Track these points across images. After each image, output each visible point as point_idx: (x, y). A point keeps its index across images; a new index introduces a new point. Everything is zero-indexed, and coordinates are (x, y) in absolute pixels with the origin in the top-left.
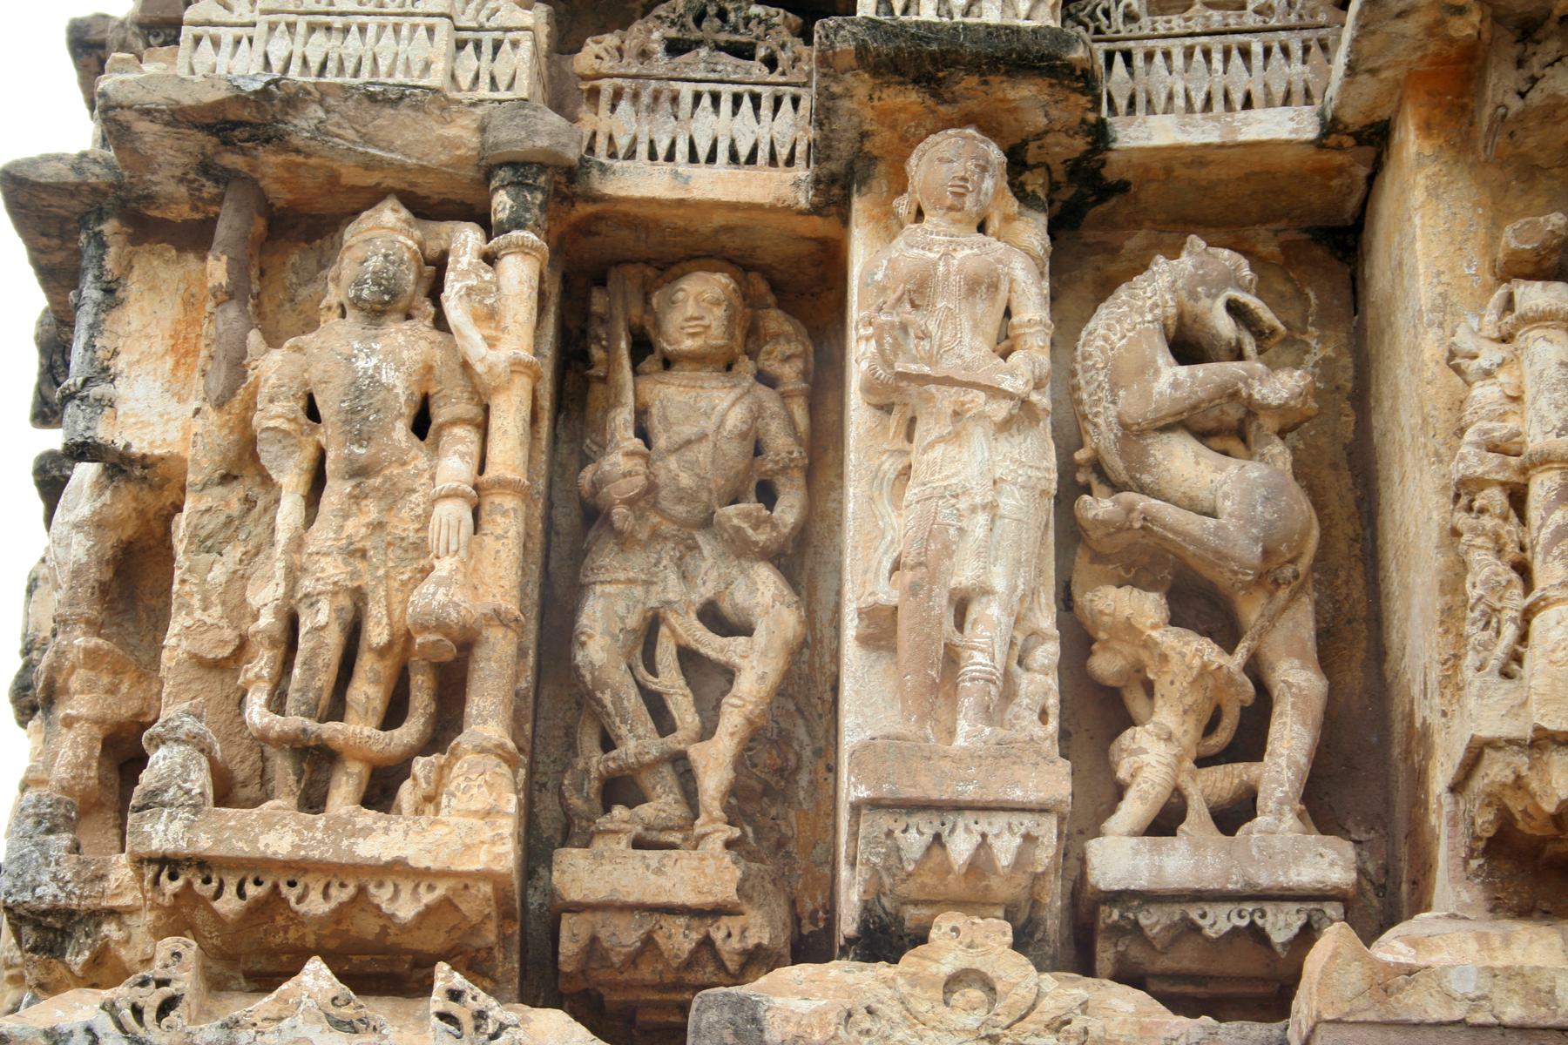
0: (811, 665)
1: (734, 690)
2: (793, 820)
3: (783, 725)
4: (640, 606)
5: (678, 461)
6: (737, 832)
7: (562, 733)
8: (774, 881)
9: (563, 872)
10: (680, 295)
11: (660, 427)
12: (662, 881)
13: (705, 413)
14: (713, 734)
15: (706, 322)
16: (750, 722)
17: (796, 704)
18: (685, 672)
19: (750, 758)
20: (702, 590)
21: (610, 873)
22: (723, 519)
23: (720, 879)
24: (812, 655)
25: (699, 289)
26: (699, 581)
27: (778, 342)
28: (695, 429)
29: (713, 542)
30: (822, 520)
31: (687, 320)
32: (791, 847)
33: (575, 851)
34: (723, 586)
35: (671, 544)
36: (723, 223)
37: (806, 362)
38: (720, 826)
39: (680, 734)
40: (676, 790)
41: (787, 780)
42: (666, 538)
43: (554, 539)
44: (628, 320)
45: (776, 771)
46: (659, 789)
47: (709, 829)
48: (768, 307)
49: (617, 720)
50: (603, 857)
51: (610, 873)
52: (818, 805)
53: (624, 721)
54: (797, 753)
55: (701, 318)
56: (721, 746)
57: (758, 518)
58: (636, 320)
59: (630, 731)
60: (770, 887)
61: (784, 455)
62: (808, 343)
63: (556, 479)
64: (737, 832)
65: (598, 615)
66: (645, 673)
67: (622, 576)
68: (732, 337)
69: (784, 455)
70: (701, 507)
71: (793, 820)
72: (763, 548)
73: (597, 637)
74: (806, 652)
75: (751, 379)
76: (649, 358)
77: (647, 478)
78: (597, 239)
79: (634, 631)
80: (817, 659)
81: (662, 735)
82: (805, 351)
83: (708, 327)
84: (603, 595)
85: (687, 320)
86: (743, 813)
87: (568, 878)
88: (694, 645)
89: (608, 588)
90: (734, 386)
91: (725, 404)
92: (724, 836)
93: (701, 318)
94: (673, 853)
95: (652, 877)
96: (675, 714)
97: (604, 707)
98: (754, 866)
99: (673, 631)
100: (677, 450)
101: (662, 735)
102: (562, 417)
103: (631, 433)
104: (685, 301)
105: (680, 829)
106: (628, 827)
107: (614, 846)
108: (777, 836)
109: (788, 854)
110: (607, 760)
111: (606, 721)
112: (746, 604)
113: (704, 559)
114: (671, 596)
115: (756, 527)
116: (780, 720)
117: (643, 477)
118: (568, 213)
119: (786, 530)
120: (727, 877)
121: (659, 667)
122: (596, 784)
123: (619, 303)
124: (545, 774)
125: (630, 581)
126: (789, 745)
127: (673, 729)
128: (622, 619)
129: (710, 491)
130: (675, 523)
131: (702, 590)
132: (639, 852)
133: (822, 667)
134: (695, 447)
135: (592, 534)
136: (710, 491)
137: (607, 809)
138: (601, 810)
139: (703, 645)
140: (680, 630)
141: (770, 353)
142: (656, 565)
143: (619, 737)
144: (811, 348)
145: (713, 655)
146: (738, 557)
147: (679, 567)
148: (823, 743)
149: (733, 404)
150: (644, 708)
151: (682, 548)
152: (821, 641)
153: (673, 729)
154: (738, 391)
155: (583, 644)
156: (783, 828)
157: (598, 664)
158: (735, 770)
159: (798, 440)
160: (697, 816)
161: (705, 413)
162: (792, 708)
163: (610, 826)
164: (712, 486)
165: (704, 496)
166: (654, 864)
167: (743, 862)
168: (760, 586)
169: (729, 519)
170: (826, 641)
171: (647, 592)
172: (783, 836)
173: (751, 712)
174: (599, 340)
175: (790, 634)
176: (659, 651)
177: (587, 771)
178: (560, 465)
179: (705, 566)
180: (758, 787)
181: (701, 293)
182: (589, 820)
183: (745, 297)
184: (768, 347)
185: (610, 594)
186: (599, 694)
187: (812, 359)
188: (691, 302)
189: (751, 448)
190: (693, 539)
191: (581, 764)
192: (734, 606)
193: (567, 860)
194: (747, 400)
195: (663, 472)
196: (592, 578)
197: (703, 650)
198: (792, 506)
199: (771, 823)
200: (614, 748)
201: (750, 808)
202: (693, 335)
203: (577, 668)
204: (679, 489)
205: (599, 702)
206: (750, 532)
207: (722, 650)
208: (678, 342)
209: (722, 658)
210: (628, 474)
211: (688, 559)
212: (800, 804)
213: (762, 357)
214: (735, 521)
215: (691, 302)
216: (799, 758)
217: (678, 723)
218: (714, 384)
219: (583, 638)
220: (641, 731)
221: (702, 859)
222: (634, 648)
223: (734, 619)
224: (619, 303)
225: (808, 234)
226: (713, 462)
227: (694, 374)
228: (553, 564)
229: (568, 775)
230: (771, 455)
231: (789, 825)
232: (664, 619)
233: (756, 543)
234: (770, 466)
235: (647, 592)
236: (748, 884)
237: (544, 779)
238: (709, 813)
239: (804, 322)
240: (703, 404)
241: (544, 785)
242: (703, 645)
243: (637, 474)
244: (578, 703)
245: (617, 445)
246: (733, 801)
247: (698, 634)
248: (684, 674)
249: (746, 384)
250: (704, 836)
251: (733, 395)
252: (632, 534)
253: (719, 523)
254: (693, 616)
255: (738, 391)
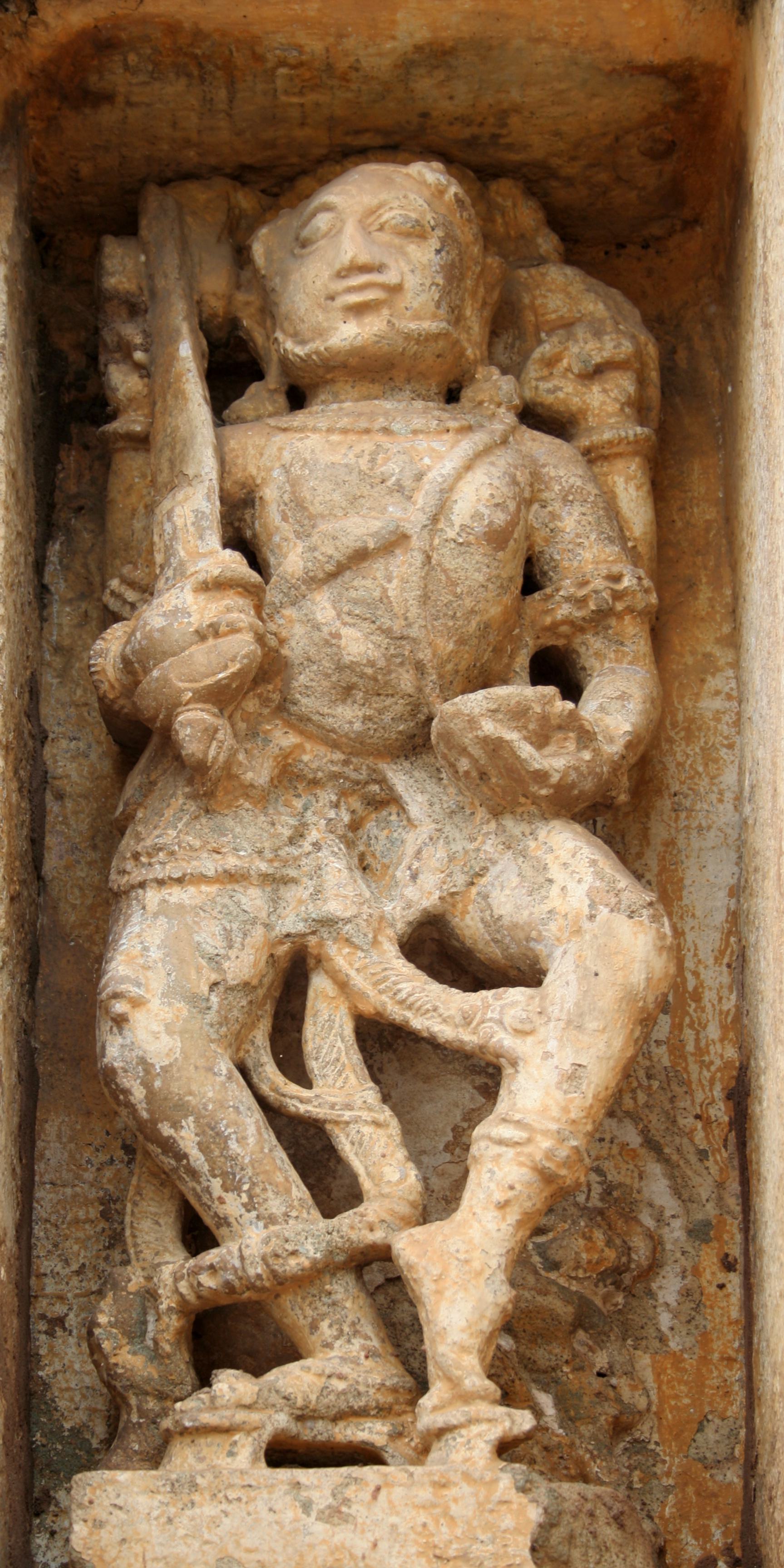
0: (676, 1048)
1: (502, 1105)
2: (649, 1376)
3: (613, 1176)
4: (259, 932)
5: (335, 603)
6: (524, 1421)
7: (94, 1212)
8: (618, 1520)
9: (99, 1524)
10: (322, 221)
11: (287, 529)
12: (343, 1535)
13: (399, 488)
14: (533, 1549)
15: (390, 277)
16: (546, 1177)
17: (645, 1132)
18: (375, 1072)
19: (541, 1250)
20: (411, 892)
21: (214, 1522)
22: (456, 726)
23: (488, 1526)
24: (678, 1027)
25: (368, 200)
26: (402, 874)
27: (571, 336)
28: (376, 525)
29: (431, 786)
30: (689, 738)
31: (341, 275)
32: (645, 1430)
33: (123, 1476)
34: (461, 879)
35: (328, 795)
36: (422, 35)
37: (641, 382)
38: (484, 1409)
39: (370, 1209)
40: (368, 1329)
41: (630, 1293)
42: (314, 783)
43: (53, 806)
44: (198, 304)
45: (603, 1276)
46: (326, 1329)
47: (454, 1415)
48: (542, 261)
49: (216, 1184)
50: (194, 1486)
51: (214, 1522)
52: (705, 1339)
53: (232, 1185)
54: (650, 1236)
55: (379, 268)
56: (475, 1232)
57: (544, 718)
58: (216, 305)
59: (249, 1207)
60: (609, 1533)
61: (598, 583)
62: (644, 337)
63: (49, 679)
64: (524, 1421)
65: (155, 954)
66: (279, 1079)
67: (209, 865)
68: (457, 318)
69: (598, 583)
70: (399, 707)
71: (649, 1376)
72: (559, 788)
73: (155, 1004)
74: (665, 1022)
75: (510, 419)
76: (254, 388)
77: (260, 639)
78: (107, 116)
79: (246, 986)
80: (689, 1035)
81: (328, 1213)
82: (639, 354)
83: (396, 289)
84: (164, 909)
85: (341, 275)
86: (529, 1365)
87: (108, 1537)
88: (396, 1013)
89: (176, 895)
90: (468, 429)
91: (449, 466)
92: (495, 1433)
93: (379, 268)
94: (370, 1473)
95: (320, 1529)
96: (357, 1165)
97: (181, 1156)
98: (570, 1490)
99: (343, 985)
100: (332, 576)
101: (328, 1213)
102: (55, 548)
103: (214, 540)
104: (334, 232)
105: (382, 1411)
106: (255, 1417)
107: (223, 1462)
108: (611, 1410)
109: (640, 1448)
110: (195, 1272)
111: (188, 1186)
112: (524, 916)
113: (411, 823)
114: (334, 907)
115: (541, 740)
116: (607, 1165)
117: (247, 637)
118: (22, 35)
119: (614, 749)
120: (508, 1522)
121: (313, 1065)
122: (174, 1322)
123: (171, 260)
124: (61, 1298)
125: (231, 877)
126: (631, 1218)
127: (355, 1197)
128: (214, 960)
129: (420, 668)
130: (335, 746)
131: (411, 892)
132: (284, 1474)
133: (700, 1051)
134: (378, 567)
135: (135, 779)
136: (420, 668)
137: (204, 1381)
138: (189, 1377)
139: (419, 1011)
140: (358, 981)
141: (550, 363)
142: (291, 841)
143: (224, 1221)
144: (652, 350)
145: (445, 1032)
146: (496, 813)
147: (350, 844)
148: (711, 1210)
149: (468, 467)
150: (281, 1155)
151: (355, 803)
152: (697, 997)
153: (355, 1197)
154: (479, 439)
155: (120, 1021)
156: (626, 1394)
157: (159, 1063)
158: (512, 1283)
159: (633, 556)
160: (422, 1386)
161: (399, 488)
162: (633, 1138)
163: (208, 1418)
164: (425, 655)
165: (406, 680)
166: (322, 1499)
167: (542, 1487)
168: (555, 872)
169: (472, 722)
170: (709, 996)
171: (275, 901)
172: (626, 1408)
173: (549, 1155)
174: (125, 350)
175: (638, 977)
176: (310, 1030)
177: (150, 1295)
178: (58, 649)
179: (412, 840)
180: (565, 1311)
181: (372, 212)
182: (161, 1396)
183: (489, 240)
184: (546, 349)
185: (180, 907)
186: (166, 1130)
187: (654, 375)
188: (350, 228)
189: (515, 570)
190: (382, 781)
191: (136, 1280)
192: (494, 922)
193: (104, 1499)
194: (503, 460)
195: (299, 630)
196: (137, 875)
197: (418, 1023)
198: (623, 697)
199: (597, 1384)
200: (214, 1243)
201: (542, 1355)
202: (359, 310)
203: (110, 1073)
204: (340, 668)
205: (169, 1147)
206: (526, 750)
207: (467, 1020)
208: (321, 333)
209: (468, 1038)
210: (214, 631)
211: (371, 827)
212: (663, 1339)
213: (532, 371)
214: (489, 727)
215: (350, 228)
216: (656, 1242)
217: (366, 1184)
218: (418, 422)
219: (119, 1007)
220: (275, 1206)
221: (442, 1485)
222: (249, 1026)
223: (495, 952)
224: (171, 260)
225: (646, 56)
226: (425, 599)
227: (364, 406)
228: (52, 864)
229: (106, 1304)
230: (568, 587)
231: (638, 1384)
232: (319, 960)
233: (541, 776)
234: (564, 610)
235: (275, 901)
236: (557, 1535)
237: (59, 1309)
238: (453, 1382)
239: (636, 297)
240: (393, 467)
241: (60, 1321)
242: (419, 1011)
243: (234, 630)
244: (129, 1149)
245: (181, 572)
246: (507, 1343)
247: (406, 987)
248: (376, 1081)
249: (498, 427)
250: (441, 1433)
251: (467, 446)
252: (229, 771)
253: (447, 736)
254: (391, 951)
255: (479, 439)
